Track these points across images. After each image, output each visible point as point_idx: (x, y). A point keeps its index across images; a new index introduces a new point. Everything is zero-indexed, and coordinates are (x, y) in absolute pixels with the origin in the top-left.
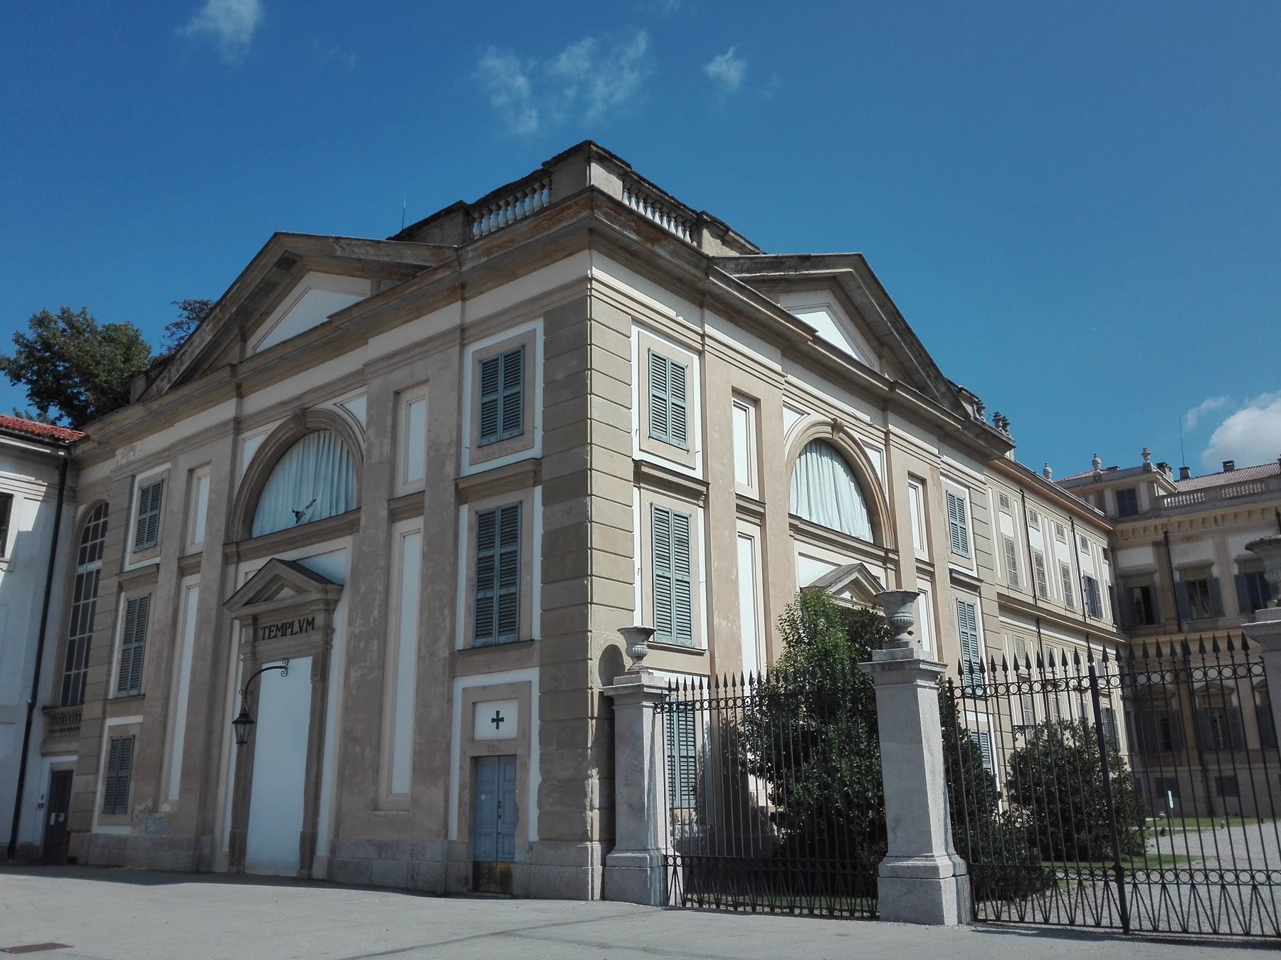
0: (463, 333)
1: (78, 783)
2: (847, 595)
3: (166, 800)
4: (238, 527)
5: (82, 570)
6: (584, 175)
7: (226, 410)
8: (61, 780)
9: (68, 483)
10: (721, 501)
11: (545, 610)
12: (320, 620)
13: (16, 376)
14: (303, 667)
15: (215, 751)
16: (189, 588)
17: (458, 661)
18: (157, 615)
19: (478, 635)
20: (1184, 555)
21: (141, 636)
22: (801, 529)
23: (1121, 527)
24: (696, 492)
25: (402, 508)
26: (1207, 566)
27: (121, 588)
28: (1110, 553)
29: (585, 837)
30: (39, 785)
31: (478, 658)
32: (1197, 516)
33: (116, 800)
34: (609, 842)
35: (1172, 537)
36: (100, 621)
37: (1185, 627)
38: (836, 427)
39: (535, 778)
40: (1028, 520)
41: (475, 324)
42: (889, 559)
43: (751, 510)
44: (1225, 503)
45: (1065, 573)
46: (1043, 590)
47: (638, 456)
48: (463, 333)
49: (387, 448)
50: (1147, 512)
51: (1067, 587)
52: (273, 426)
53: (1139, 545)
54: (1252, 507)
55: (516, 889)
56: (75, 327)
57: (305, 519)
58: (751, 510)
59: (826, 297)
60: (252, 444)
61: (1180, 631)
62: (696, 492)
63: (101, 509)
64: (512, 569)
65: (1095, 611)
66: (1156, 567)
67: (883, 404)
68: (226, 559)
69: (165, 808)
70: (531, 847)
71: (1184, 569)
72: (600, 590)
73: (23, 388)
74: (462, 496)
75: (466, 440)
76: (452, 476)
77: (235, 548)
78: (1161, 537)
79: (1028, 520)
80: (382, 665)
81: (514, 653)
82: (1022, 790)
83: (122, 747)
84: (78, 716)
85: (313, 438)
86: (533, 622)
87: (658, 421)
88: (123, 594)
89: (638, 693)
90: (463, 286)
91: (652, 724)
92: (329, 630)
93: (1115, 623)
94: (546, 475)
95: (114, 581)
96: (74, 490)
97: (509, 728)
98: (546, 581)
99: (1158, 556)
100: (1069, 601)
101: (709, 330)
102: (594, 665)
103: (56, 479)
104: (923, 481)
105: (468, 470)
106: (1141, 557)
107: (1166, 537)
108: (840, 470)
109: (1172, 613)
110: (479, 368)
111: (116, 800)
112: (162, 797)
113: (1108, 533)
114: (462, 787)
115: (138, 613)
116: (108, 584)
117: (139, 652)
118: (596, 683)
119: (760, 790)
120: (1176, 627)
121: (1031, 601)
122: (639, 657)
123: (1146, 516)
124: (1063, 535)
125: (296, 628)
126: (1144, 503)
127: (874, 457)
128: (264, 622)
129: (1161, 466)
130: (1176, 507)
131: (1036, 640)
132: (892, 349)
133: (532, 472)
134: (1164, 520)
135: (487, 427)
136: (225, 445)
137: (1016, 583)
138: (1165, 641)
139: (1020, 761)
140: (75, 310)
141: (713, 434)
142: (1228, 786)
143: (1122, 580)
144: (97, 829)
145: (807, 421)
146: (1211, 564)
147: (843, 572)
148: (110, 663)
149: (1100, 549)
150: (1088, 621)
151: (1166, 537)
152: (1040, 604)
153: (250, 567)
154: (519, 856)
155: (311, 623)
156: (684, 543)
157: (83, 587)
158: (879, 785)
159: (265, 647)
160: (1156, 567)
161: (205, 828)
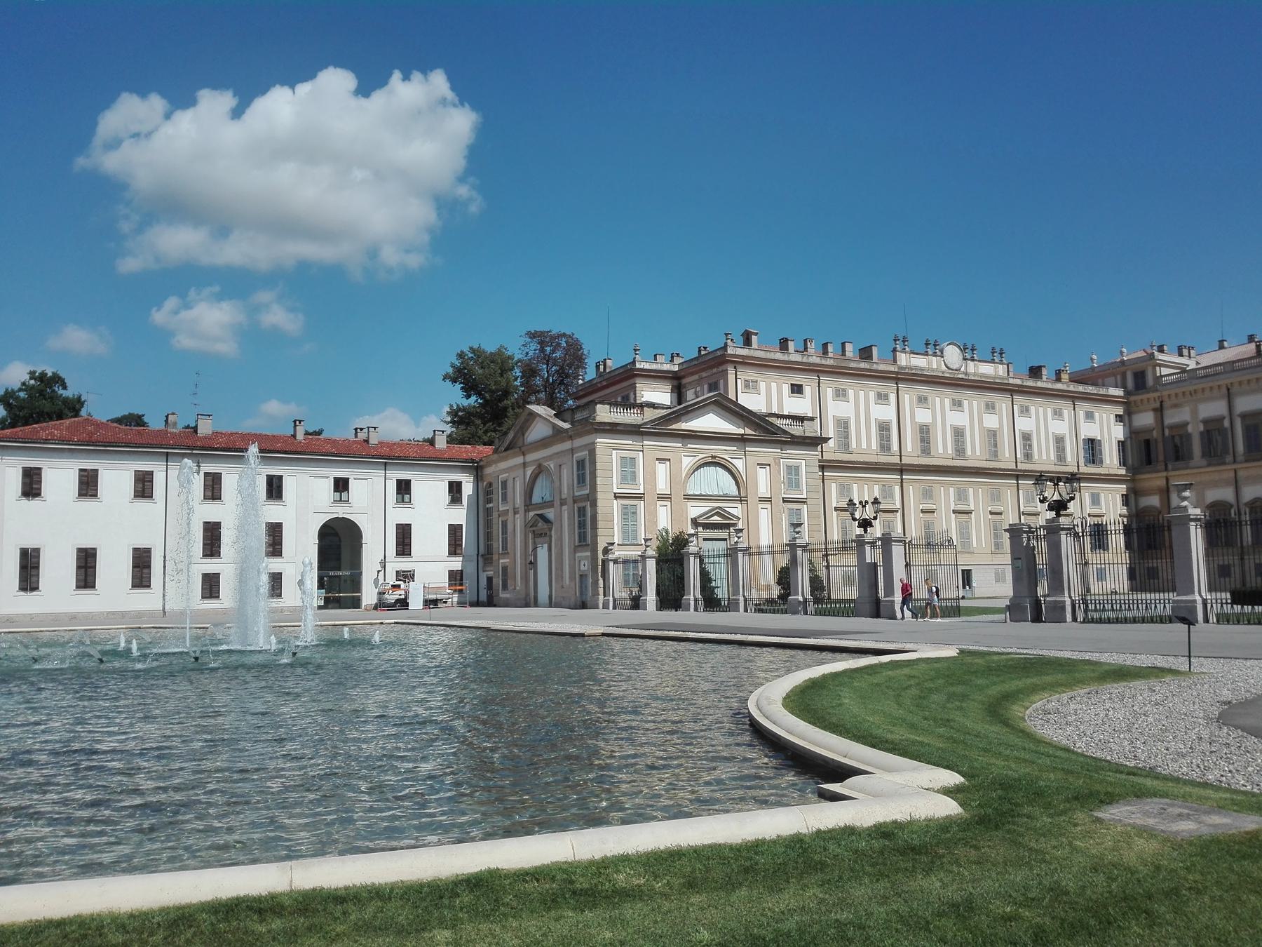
1: (494, 581)
5: (488, 506)
7: (520, 460)
8: (490, 580)
9: (479, 474)
13: (454, 381)
14: (546, 546)
18: (510, 527)
20: (1172, 418)
21: (506, 534)
23: (1132, 398)
25: (563, 502)
27: (499, 516)
30: (483, 582)
33: (505, 587)
35: (1165, 405)
36: (495, 527)
37: (1170, 467)
41: (577, 448)
44: (1197, 381)
47: (616, 491)
48: (572, 451)
53: (1146, 411)
56: (477, 352)
59: (712, 407)
60: (529, 472)
61: (1166, 469)
62: (640, 497)
63: (490, 484)
66: (1154, 425)
68: (525, 511)
69: (518, 588)
71: (1171, 427)
73: (458, 386)
74: (575, 502)
78: (1158, 405)
83: (505, 569)
84: (492, 558)
92: (551, 536)
94: (590, 499)
95: (497, 513)
96: (482, 476)
97: (586, 568)
99: (1156, 418)
103: (475, 473)
105: (576, 494)
106: (1145, 419)
107: (1161, 405)
109: (1161, 458)
111: (505, 587)
115: (505, 524)
116: (495, 514)
117: (506, 538)
120: (1163, 467)
126: (1150, 381)
136: (521, 471)
137: (996, 456)
138: (1155, 480)
140: (476, 347)
143: (1132, 433)
144: (501, 595)
145: (698, 458)
146: (1188, 424)
151: (1161, 405)
153: (532, 514)
157: (488, 512)
160: (1154, 425)
161: (527, 595)
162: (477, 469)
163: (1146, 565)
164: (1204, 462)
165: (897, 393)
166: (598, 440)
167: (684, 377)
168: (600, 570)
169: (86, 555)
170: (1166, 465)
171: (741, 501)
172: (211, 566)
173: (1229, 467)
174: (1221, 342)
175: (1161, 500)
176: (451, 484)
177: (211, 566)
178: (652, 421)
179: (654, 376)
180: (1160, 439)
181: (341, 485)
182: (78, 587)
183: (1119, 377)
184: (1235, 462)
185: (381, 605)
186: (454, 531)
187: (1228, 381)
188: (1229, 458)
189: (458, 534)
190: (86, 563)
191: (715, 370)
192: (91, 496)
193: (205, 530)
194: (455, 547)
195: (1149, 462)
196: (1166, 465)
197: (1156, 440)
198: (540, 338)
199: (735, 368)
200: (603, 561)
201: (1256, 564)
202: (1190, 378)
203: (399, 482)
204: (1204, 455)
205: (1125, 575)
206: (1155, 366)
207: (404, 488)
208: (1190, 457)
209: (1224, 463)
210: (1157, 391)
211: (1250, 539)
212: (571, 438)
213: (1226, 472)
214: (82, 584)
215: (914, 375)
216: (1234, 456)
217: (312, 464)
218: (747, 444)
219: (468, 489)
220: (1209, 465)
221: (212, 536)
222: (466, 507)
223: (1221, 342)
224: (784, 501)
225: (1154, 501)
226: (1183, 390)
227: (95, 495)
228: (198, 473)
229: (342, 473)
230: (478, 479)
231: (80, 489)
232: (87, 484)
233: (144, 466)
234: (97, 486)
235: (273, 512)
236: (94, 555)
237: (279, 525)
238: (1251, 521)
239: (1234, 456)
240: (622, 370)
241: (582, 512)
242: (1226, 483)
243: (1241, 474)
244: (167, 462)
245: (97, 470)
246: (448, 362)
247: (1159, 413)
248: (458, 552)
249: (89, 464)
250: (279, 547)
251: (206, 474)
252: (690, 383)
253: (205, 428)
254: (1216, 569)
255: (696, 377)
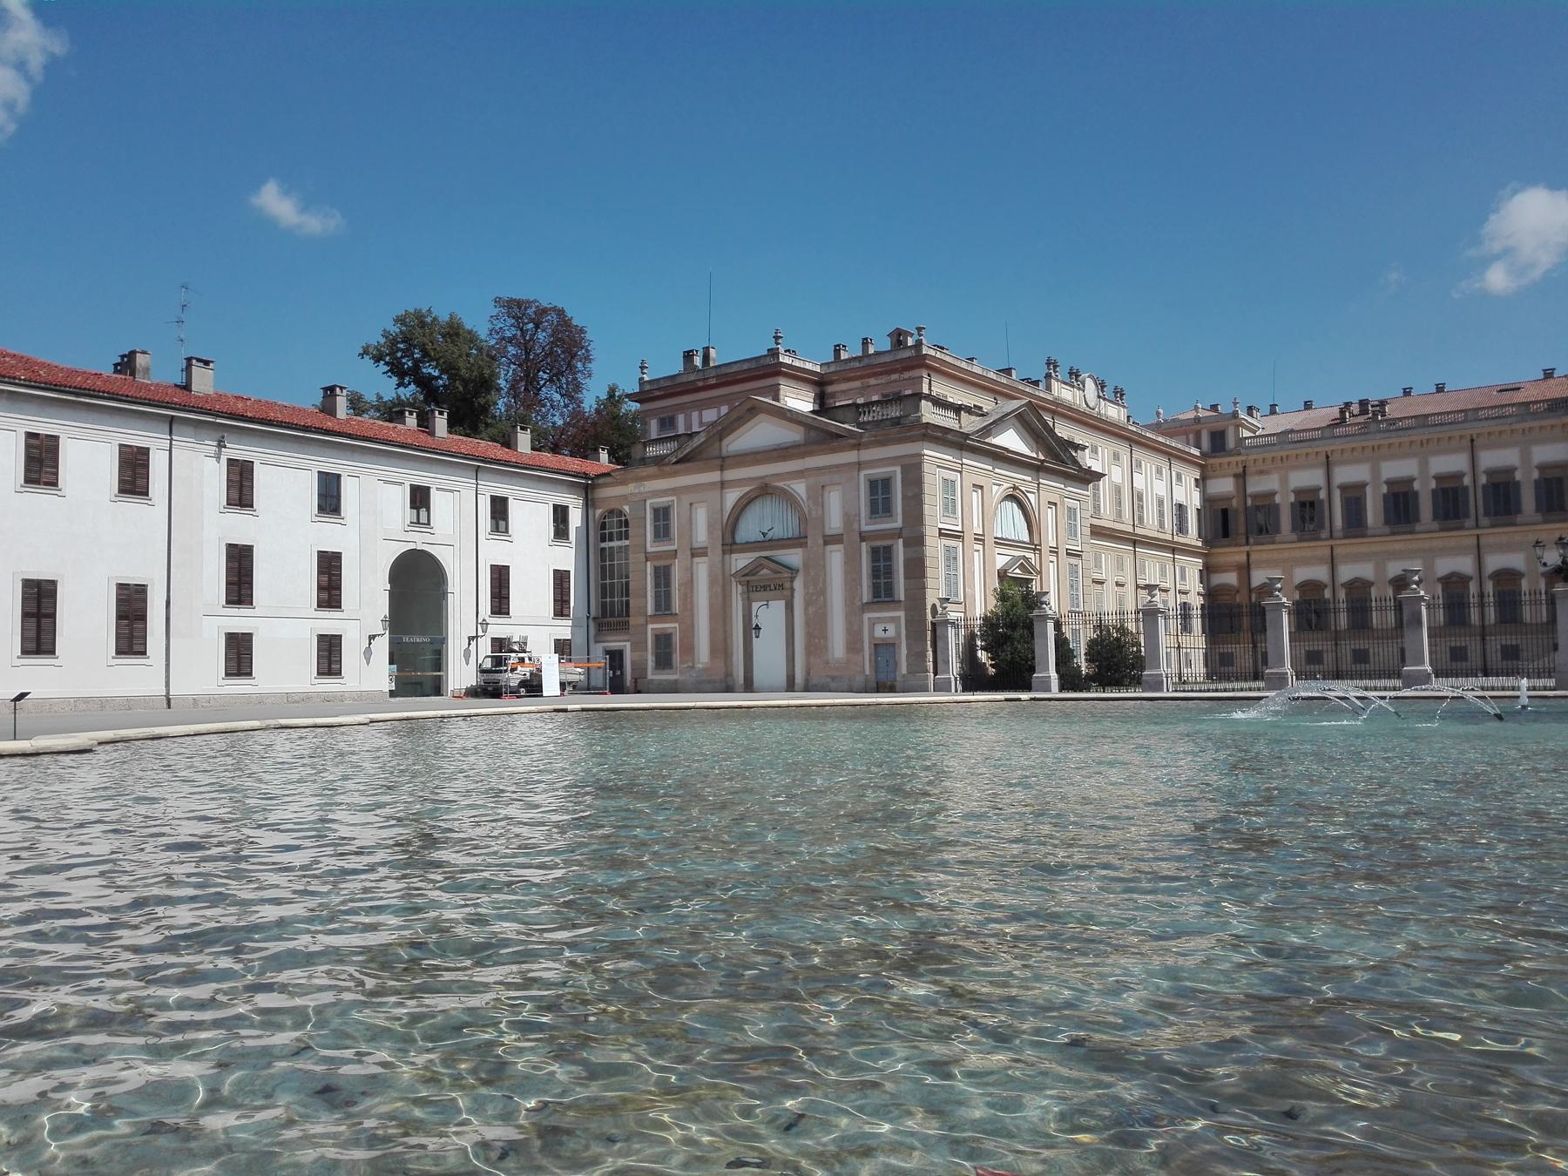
0: (860, 465)
2: (1018, 571)
3: (699, 663)
4: (728, 536)
6: (917, 409)
7: (715, 476)
9: (589, 497)
10: (969, 538)
11: (906, 590)
12: (787, 585)
14: (778, 607)
15: (729, 640)
16: (698, 563)
17: (866, 607)
19: (874, 597)
20: (1256, 485)
22: (1001, 542)
23: (1211, 461)
24: (958, 536)
26: (1272, 494)
28: (1201, 483)
29: (927, 671)
31: (875, 606)
32: (1269, 456)
34: (936, 673)
37: (1251, 540)
38: (1015, 488)
39: (904, 651)
40: (1134, 467)
42: (1036, 549)
43: (980, 539)
44: (1292, 446)
45: (1161, 503)
46: (1141, 519)
47: (941, 526)
48: (860, 465)
49: (820, 512)
50: (1232, 450)
51: (1161, 514)
52: (748, 489)
53: (1224, 476)
54: (1310, 450)
55: (897, 689)
57: (769, 536)
58: (980, 539)
62: (958, 536)
64: (889, 572)
65: (1182, 528)
67: (1037, 469)
70: (904, 676)
71: (1255, 497)
72: (930, 583)
75: (863, 515)
76: (857, 530)
77: (730, 545)
78: (1241, 470)
79: (1134, 467)
80: (825, 606)
81: (892, 605)
82: (1091, 657)
85: (769, 498)
86: (901, 593)
87: (946, 508)
88: (649, 563)
89: (947, 622)
90: (859, 445)
91: (951, 631)
92: (792, 590)
93: (1200, 537)
97: (891, 633)
98: (905, 578)
99: (1237, 485)
100: (1162, 524)
101: (965, 461)
102: (929, 611)
103: (584, 495)
104: (1055, 504)
106: (1224, 486)
107: (1244, 471)
108: (1015, 505)
109: (1242, 529)
110: (868, 483)
112: (696, 661)
113: (1201, 466)
114: (870, 655)
115: (663, 577)
118: (929, 618)
119: (982, 656)
120: (1244, 541)
121: (1169, 538)
122: (945, 608)
123: (1231, 453)
124: (1161, 474)
125: (773, 588)
126: (1231, 443)
127: (1031, 496)
128: (751, 584)
129: (1250, 410)
130: (1254, 447)
131: (1132, 557)
132: (1043, 439)
133: (898, 534)
134: (1243, 458)
135: (874, 510)
137: (1121, 517)
138: (1234, 554)
139: (1092, 644)
141: (966, 509)
142: (1361, 656)
143: (1207, 500)
145: (1003, 488)
147: (1015, 559)
148: (646, 597)
149: (1193, 480)
150: (1176, 538)
151: (1244, 471)
152: (1138, 531)
154: (898, 679)
155: (782, 586)
156: (955, 558)
158: (1033, 652)
159: (753, 595)
160: (1235, 493)
162: (587, 488)
163: (1448, 644)
164: (1294, 537)
165: (170, 451)
166: (926, 452)
167: (831, 383)
168: (929, 638)
169: (39, 594)
170: (1247, 539)
171: (1034, 550)
172: (329, 623)
173: (1242, 549)
174: (1273, 406)
175: (1240, 578)
176: (556, 507)
177: (329, 623)
178: (978, 431)
179: (799, 377)
180: (1241, 509)
181: (420, 498)
182: (25, 652)
183: (1191, 437)
184: (1331, 537)
185: (488, 689)
186: (561, 578)
187: (1329, 449)
188: (1325, 534)
189: (565, 585)
190: (39, 607)
191: (894, 377)
192: (47, 484)
193: (230, 558)
194: (561, 609)
195: (1226, 534)
196: (1247, 539)
197: (1236, 511)
198: (515, 308)
199: (929, 375)
200: (933, 624)
201: (1502, 646)
202: (1280, 443)
203: (494, 499)
204: (1294, 529)
205: (1202, 662)
206: (1237, 426)
207: (499, 509)
208: (1277, 530)
209: (1318, 539)
210: (1239, 454)
211: (1442, 619)
212: (858, 446)
213: (1321, 549)
214: (33, 646)
215: (1070, 409)
216: (1331, 531)
217: (411, 464)
218: (1041, 474)
219: (575, 518)
220: (1300, 540)
221: (240, 568)
222: (573, 545)
223: (1273, 406)
224: (1067, 554)
225: (1231, 578)
226: (1273, 454)
227: (54, 484)
228: (218, 458)
229: (422, 478)
230: (588, 505)
231: (28, 470)
232: (40, 461)
233: (137, 437)
234: (56, 467)
235: (330, 535)
236: (52, 594)
237: (337, 557)
238: (1444, 604)
239: (1331, 531)
240: (746, 366)
241: (881, 556)
242: (1320, 561)
243: (1337, 551)
244: (171, 434)
245: (56, 438)
246: (378, 326)
247: (1242, 479)
248: (565, 612)
249: (45, 425)
250: (337, 592)
251: (231, 462)
252: (843, 392)
253: (204, 383)
254: (1303, 656)
255: (857, 384)
